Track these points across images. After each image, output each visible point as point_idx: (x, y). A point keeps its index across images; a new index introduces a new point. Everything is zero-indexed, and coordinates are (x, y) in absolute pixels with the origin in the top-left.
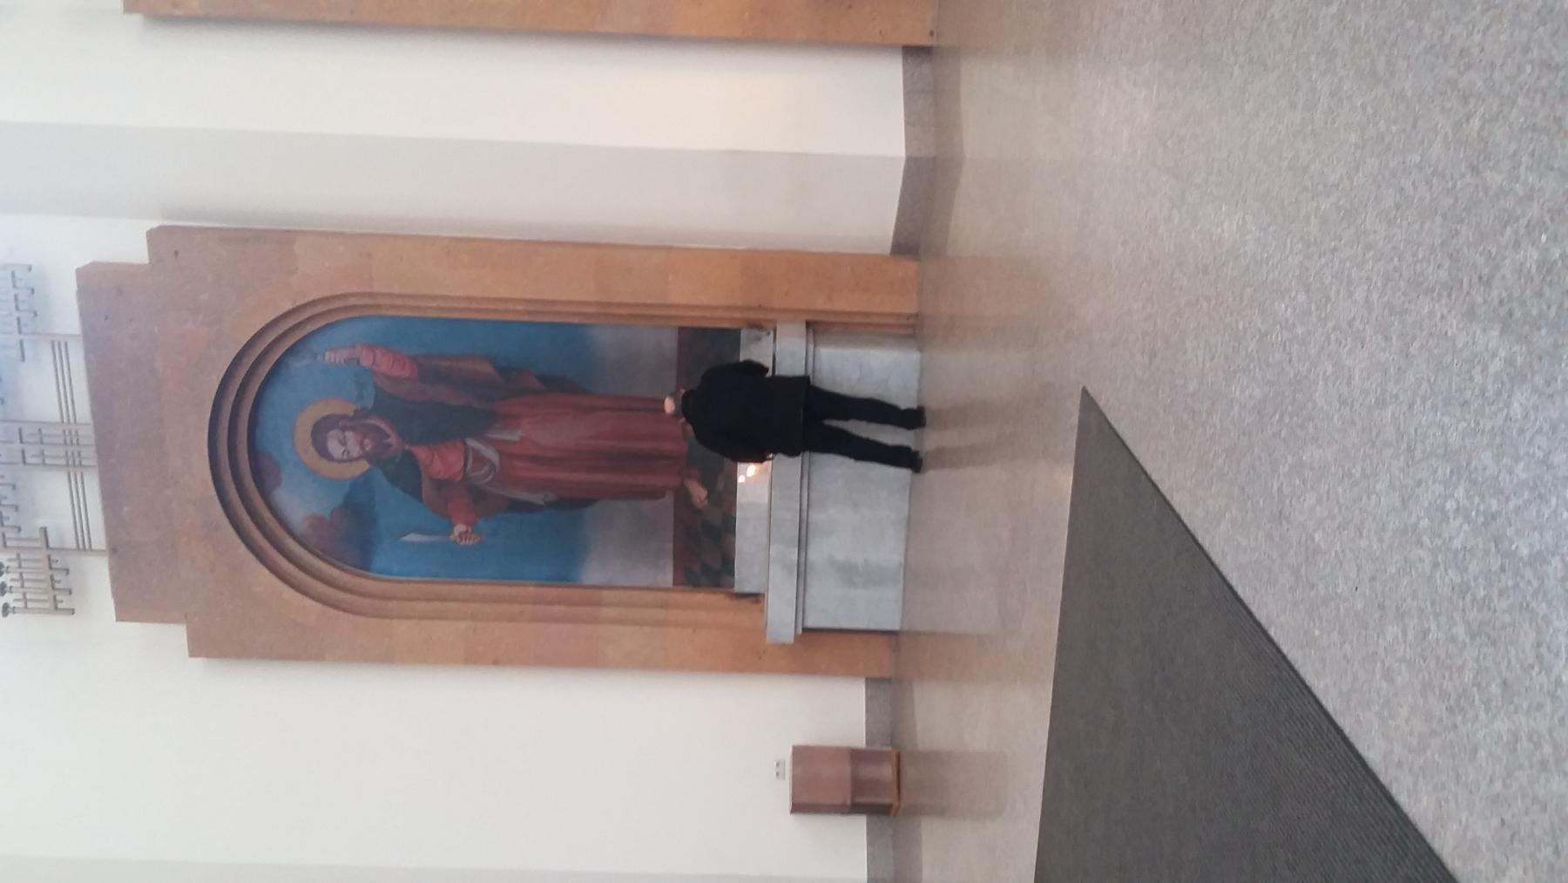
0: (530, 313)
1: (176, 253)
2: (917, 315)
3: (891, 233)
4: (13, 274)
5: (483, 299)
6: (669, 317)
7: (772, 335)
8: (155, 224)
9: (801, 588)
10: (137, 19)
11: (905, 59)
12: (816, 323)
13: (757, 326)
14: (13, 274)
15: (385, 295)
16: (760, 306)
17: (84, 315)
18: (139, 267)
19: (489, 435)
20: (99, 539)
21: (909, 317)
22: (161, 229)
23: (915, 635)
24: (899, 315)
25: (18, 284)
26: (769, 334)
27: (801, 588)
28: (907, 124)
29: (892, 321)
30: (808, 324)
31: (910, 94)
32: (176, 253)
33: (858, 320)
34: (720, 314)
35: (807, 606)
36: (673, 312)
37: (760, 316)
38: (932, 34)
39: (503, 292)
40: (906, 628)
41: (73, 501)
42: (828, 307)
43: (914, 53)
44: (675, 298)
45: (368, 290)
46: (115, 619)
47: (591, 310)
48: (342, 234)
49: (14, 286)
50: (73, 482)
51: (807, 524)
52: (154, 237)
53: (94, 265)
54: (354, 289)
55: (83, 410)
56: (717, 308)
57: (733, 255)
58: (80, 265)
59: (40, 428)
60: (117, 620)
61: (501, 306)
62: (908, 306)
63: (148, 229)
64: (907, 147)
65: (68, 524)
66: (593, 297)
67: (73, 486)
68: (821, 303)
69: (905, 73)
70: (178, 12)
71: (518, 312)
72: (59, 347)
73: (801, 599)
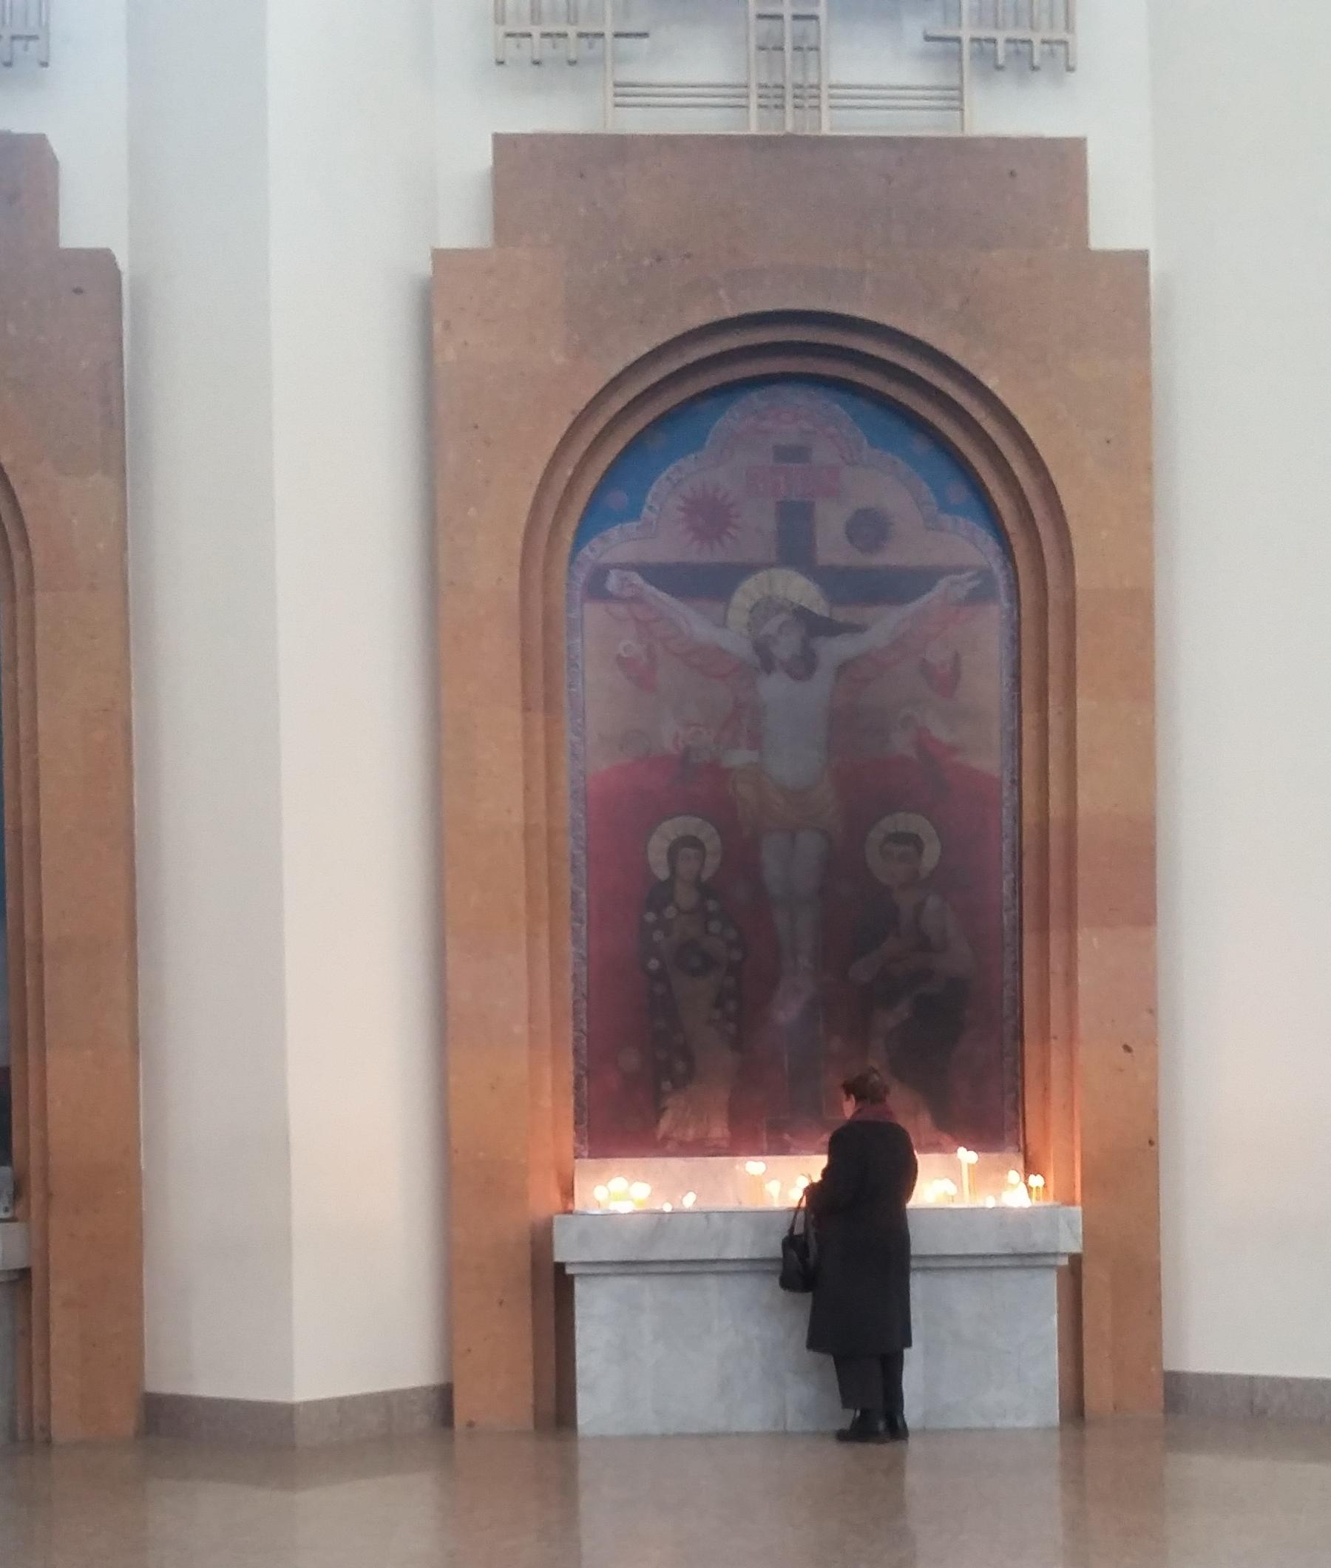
0: (18, 831)
1: (78, 291)
2: (48, 1442)
3: (207, 1387)
4: (35, 38)
5: (35, 764)
6: (24, 1049)
7: (8, 1215)
8: (123, 261)
9: (731, 1267)
10: (426, 268)
11: (435, 1389)
12: (28, 1288)
13: (18, 1191)
14: (35, 38)
15: (31, 607)
16: (51, 1194)
17: (1002, 143)
18: (55, 234)
19: (990, 762)
20: (635, 122)
21: (46, 1429)
22: (117, 275)
23: (568, 1465)
24: (46, 1413)
25: (18, 45)
26: (6, 1210)
27: (731, 1267)
28: (342, 1401)
29: (37, 1401)
30: (25, 1273)
31: (384, 1402)
32: (78, 291)
33: (37, 1354)
34: (34, 1133)
35: (996, 1274)
36: (33, 1061)
37: (36, 1197)
38: (471, 1424)
39: (48, 789)
40: (583, 1450)
41: (866, 88)
42: (55, 1303)
43: (443, 1399)
44: (54, 1059)
45: (37, 583)
46: (500, 130)
47: (28, 929)
48: (124, 547)
49: (13, 38)
50: (920, 93)
51: (992, 1268)
52: (102, 262)
53: (53, 164)
54: (38, 559)
55: (830, 124)
56: (44, 1129)
57: (131, 1150)
58: (49, 138)
59: (808, 49)
60: (498, 138)
61: (25, 787)
62: (64, 1425)
63: (114, 250)
64: (308, 1405)
65: (663, 74)
66: (50, 934)
67: (706, 90)
68: (60, 1289)
69: (414, 1390)
70: (437, 327)
71: (18, 812)
72: (954, 98)
73: (667, 1268)
